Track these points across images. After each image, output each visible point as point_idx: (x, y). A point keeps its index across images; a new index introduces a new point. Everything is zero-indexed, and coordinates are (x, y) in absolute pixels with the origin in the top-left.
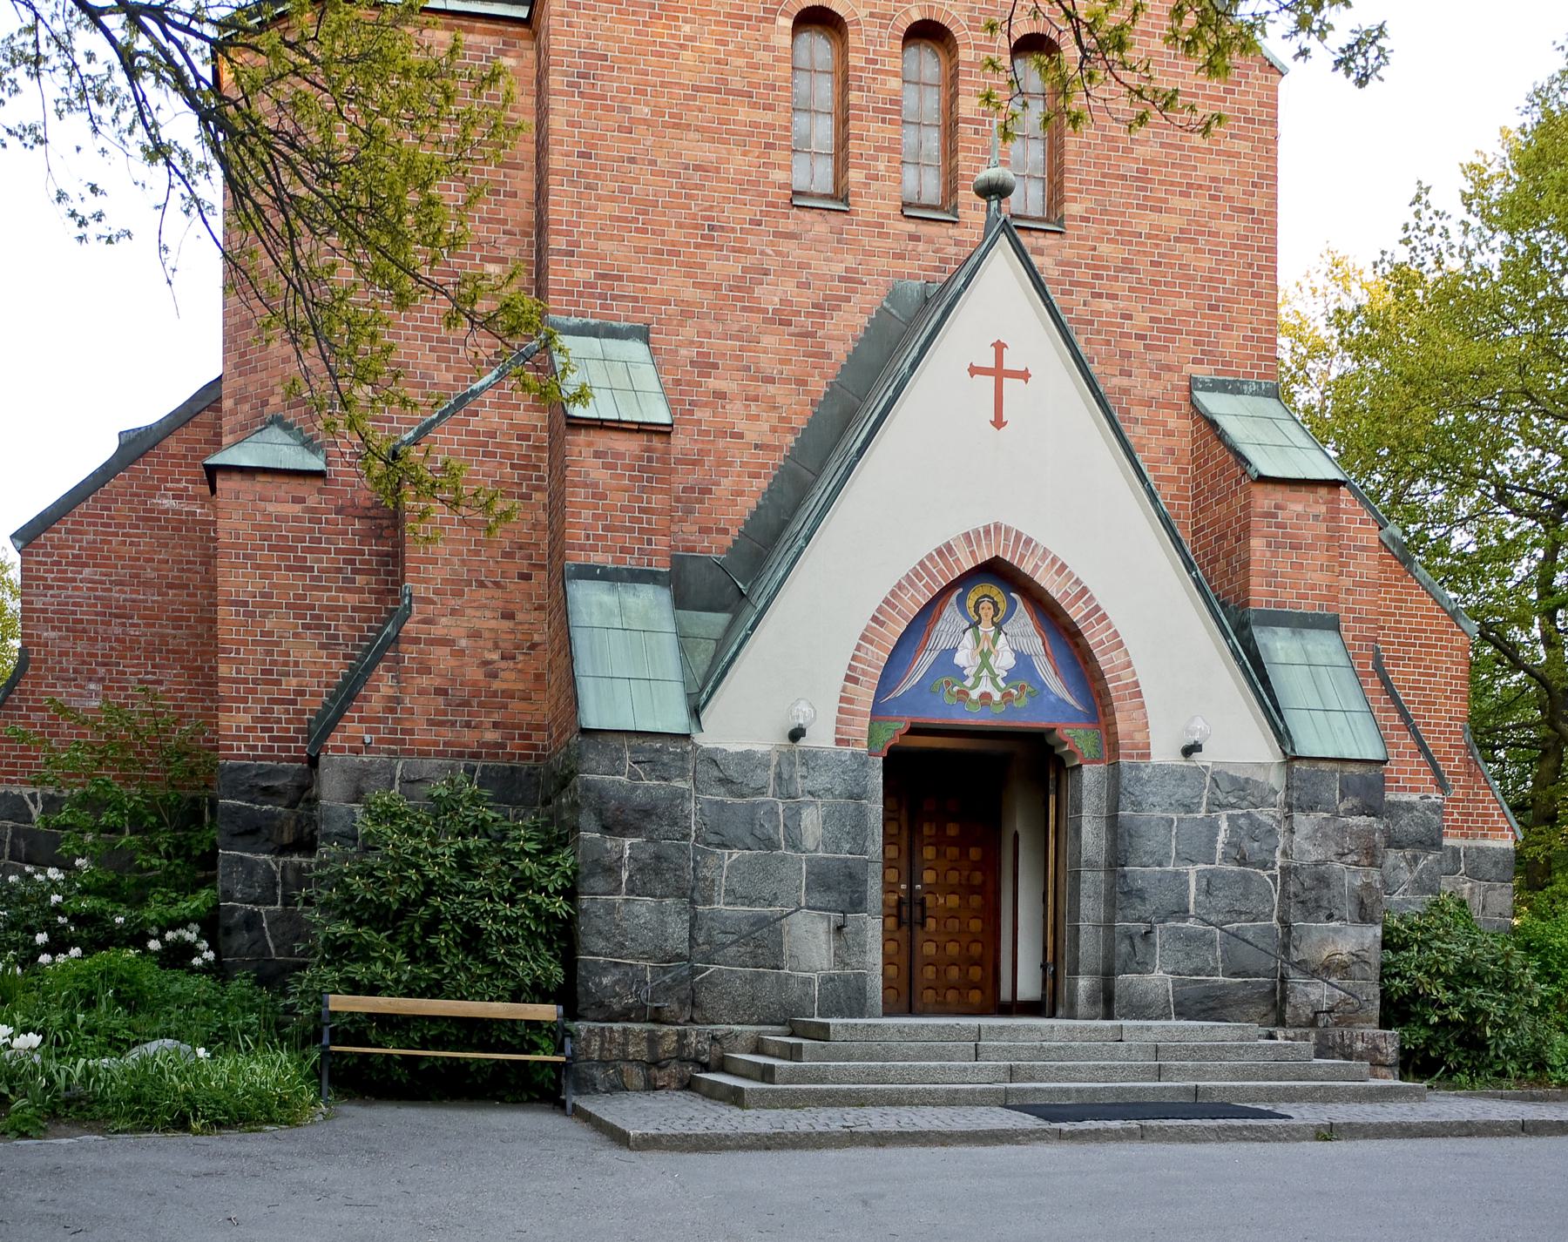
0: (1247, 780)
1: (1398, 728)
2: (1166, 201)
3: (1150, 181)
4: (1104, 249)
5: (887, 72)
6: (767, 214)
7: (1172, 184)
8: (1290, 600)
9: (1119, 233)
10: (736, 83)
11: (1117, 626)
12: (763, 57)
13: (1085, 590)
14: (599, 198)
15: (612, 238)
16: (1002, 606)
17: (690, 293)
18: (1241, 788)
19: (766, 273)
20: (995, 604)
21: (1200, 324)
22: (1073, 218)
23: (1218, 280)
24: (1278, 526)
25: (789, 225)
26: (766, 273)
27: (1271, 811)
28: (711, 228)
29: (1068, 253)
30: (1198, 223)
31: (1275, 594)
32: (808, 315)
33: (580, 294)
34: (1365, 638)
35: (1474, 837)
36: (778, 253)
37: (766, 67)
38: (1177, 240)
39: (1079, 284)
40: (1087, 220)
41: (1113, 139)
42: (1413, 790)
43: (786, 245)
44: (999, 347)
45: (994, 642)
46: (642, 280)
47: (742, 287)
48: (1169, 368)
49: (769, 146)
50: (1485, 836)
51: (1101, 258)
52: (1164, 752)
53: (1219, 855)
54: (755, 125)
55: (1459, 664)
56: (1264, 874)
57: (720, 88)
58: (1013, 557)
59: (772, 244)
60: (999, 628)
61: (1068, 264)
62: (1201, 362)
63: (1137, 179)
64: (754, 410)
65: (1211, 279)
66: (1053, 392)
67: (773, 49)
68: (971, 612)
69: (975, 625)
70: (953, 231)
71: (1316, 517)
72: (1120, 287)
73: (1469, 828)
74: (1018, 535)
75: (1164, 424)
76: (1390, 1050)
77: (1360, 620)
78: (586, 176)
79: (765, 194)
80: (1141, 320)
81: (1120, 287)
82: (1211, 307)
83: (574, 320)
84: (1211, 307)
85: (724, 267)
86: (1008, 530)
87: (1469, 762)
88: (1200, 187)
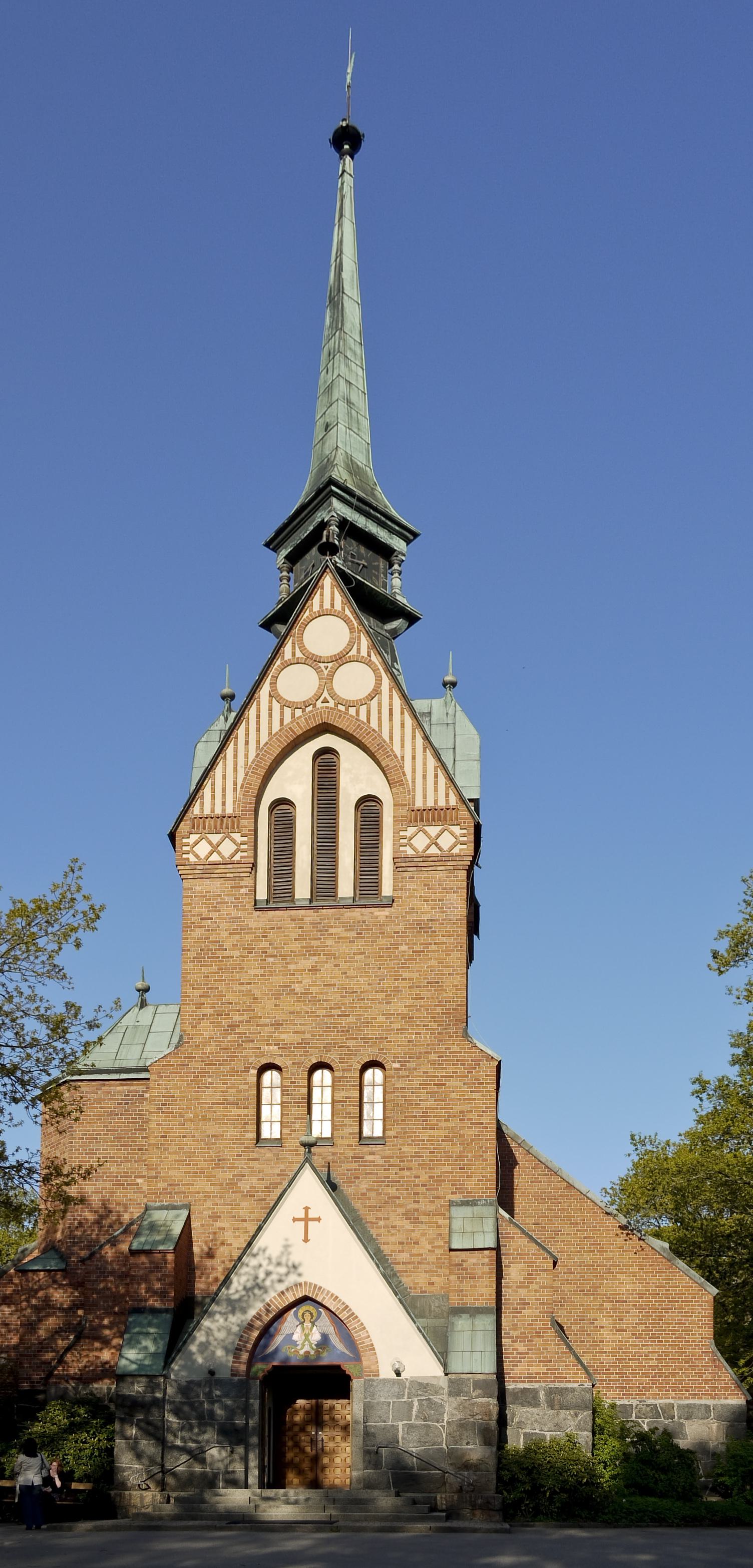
0: (427, 1384)
1: (566, 1353)
2: (437, 1124)
3: (429, 1116)
4: (405, 1149)
5: (300, 1086)
6: (244, 1151)
7: (440, 1116)
8: (469, 1302)
9: (413, 1141)
10: (231, 1099)
11: (362, 1321)
12: (243, 1087)
13: (347, 1307)
14: (169, 1153)
15: (175, 1169)
16: (315, 1314)
17: (209, 1188)
18: (423, 1387)
19: (244, 1176)
20: (311, 1314)
21: (455, 1177)
22: (390, 1137)
23: (464, 1156)
24: (463, 1269)
25: (255, 1155)
26: (244, 1176)
27: (441, 1397)
28: (219, 1160)
29: (388, 1153)
30: (453, 1132)
31: (462, 1300)
32: (262, 1191)
33: (161, 1193)
34: (546, 1312)
35: (719, 1399)
36: (249, 1167)
37: (244, 1091)
38: (442, 1140)
39: (392, 1165)
40: (397, 1137)
41: (410, 1101)
42: (574, 1382)
43: (251, 1164)
44: (307, 1209)
45: (311, 1330)
46: (188, 1185)
47: (232, 1184)
48: (438, 1197)
49: (245, 1123)
50: (726, 1398)
51: (404, 1153)
52: (386, 1373)
53: (414, 1417)
54: (239, 1115)
55: (706, 1309)
56: (438, 1425)
57: (224, 1102)
58: (313, 1293)
59: (246, 1164)
60: (313, 1324)
61: (388, 1157)
62: (456, 1193)
63: (422, 1117)
64: (237, 1234)
65: (460, 1156)
66: (332, 1223)
67: (248, 1083)
68: (300, 1318)
69: (302, 1323)
70: (330, 1149)
71: (483, 1264)
72: (413, 1165)
73: (716, 1394)
74: (315, 1286)
75: (436, 1222)
76: (497, 1504)
77: (543, 1304)
78: (164, 1145)
79: (244, 1143)
80: (424, 1177)
81: (413, 1165)
82: (460, 1168)
83: (158, 1204)
84: (460, 1168)
85: (224, 1176)
86: (311, 1284)
87: (714, 1360)
88: (455, 1116)
